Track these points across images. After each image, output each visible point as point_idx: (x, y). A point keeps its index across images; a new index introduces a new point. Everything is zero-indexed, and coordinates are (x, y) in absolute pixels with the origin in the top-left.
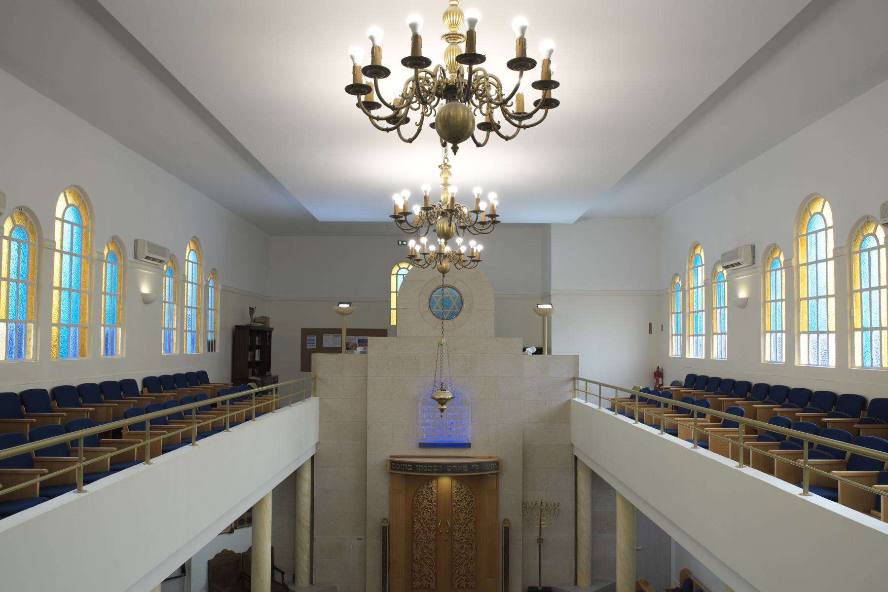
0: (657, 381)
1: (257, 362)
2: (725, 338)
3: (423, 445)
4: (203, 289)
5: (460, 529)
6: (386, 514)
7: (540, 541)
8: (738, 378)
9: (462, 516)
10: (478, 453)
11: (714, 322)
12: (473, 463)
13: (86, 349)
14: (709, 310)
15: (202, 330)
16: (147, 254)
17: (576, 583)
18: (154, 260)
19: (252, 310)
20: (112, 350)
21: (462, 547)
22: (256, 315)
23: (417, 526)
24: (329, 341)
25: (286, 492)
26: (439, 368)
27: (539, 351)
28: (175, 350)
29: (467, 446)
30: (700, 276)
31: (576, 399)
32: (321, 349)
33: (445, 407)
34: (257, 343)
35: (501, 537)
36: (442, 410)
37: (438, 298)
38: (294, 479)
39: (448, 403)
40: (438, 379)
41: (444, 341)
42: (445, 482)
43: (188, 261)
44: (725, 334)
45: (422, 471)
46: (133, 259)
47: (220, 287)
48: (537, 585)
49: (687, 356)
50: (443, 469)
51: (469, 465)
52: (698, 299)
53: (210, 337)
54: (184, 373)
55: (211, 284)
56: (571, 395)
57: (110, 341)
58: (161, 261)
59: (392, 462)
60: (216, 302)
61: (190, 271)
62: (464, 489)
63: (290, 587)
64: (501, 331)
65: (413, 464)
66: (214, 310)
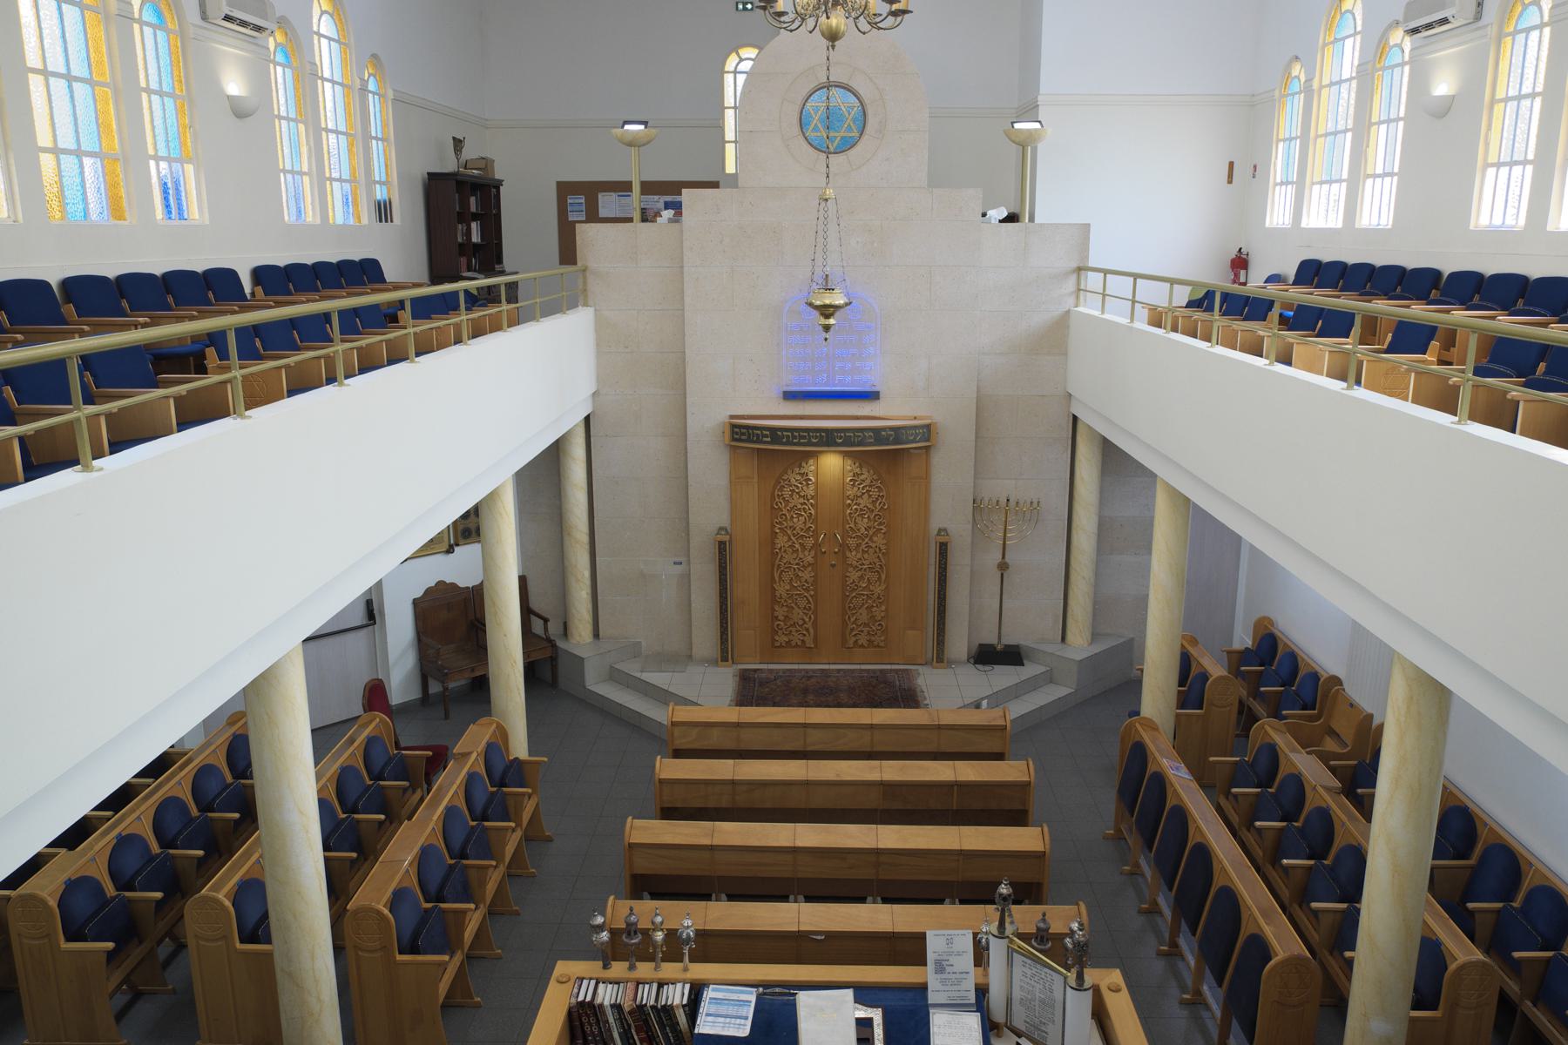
0: (1237, 276)
1: (475, 245)
2: (1391, 184)
3: (790, 396)
4: (356, 94)
5: (859, 545)
6: (723, 519)
7: (1003, 567)
8: (1410, 263)
9: (863, 524)
10: (892, 411)
11: (1370, 151)
12: (884, 429)
13: (124, 203)
14: (1362, 126)
15: (361, 176)
16: (227, 10)
17: (1063, 639)
18: (243, 24)
19: (458, 144)
20: (180, 208)
21: (861, 577)
22: (469, 153)
23: (781, 541)
24: (608, 204)
25: (543, 476)
26: (821, 233)
27: (1012, 218)
28: (311, 217)
29: (871, 396)
30: (1348, 57)
31: (1080, 309)
32: (593, 216)
33: (832, 321)
34: (473, 209)
35: (932, 561)
36: (827, 328)
37: (817, 109)
38: (554, 454)
39: (838, 314)
40: (819, 271)
41: (830, 192)
42: (831, 464)
43: (320, 35)
44: (1391, 174)
45: (789, 443)
46: (197, 20)
47: (391, 94)
48: (994, 641)
49: (1303, 225)
50: (828, 439)
51: (876, 431)
52: (1338, 107)
53: (380, 193)
54: (334, 261)
55: (372, 86)
56: (1071, 301)
57: (172, 195)
58: (258, 29)
59: (734, 426)
60: (385, 125)
61: (327, 57)
62: (866, 475)
63: (561, 644)
64: (938, 178)
65: (773, 430)
66: (382, 139)
